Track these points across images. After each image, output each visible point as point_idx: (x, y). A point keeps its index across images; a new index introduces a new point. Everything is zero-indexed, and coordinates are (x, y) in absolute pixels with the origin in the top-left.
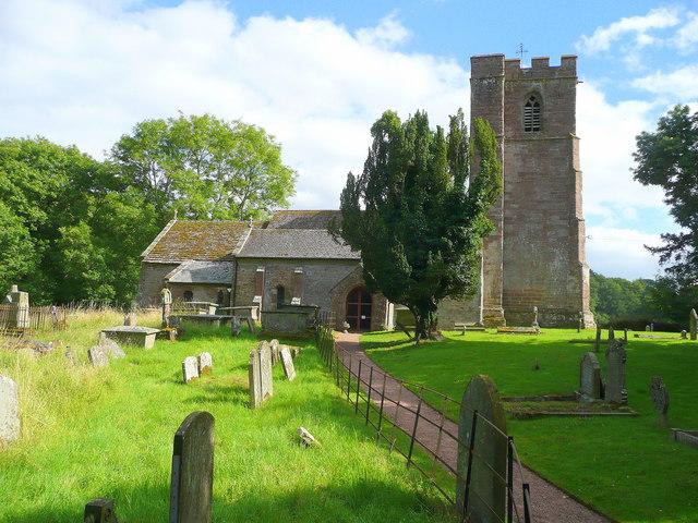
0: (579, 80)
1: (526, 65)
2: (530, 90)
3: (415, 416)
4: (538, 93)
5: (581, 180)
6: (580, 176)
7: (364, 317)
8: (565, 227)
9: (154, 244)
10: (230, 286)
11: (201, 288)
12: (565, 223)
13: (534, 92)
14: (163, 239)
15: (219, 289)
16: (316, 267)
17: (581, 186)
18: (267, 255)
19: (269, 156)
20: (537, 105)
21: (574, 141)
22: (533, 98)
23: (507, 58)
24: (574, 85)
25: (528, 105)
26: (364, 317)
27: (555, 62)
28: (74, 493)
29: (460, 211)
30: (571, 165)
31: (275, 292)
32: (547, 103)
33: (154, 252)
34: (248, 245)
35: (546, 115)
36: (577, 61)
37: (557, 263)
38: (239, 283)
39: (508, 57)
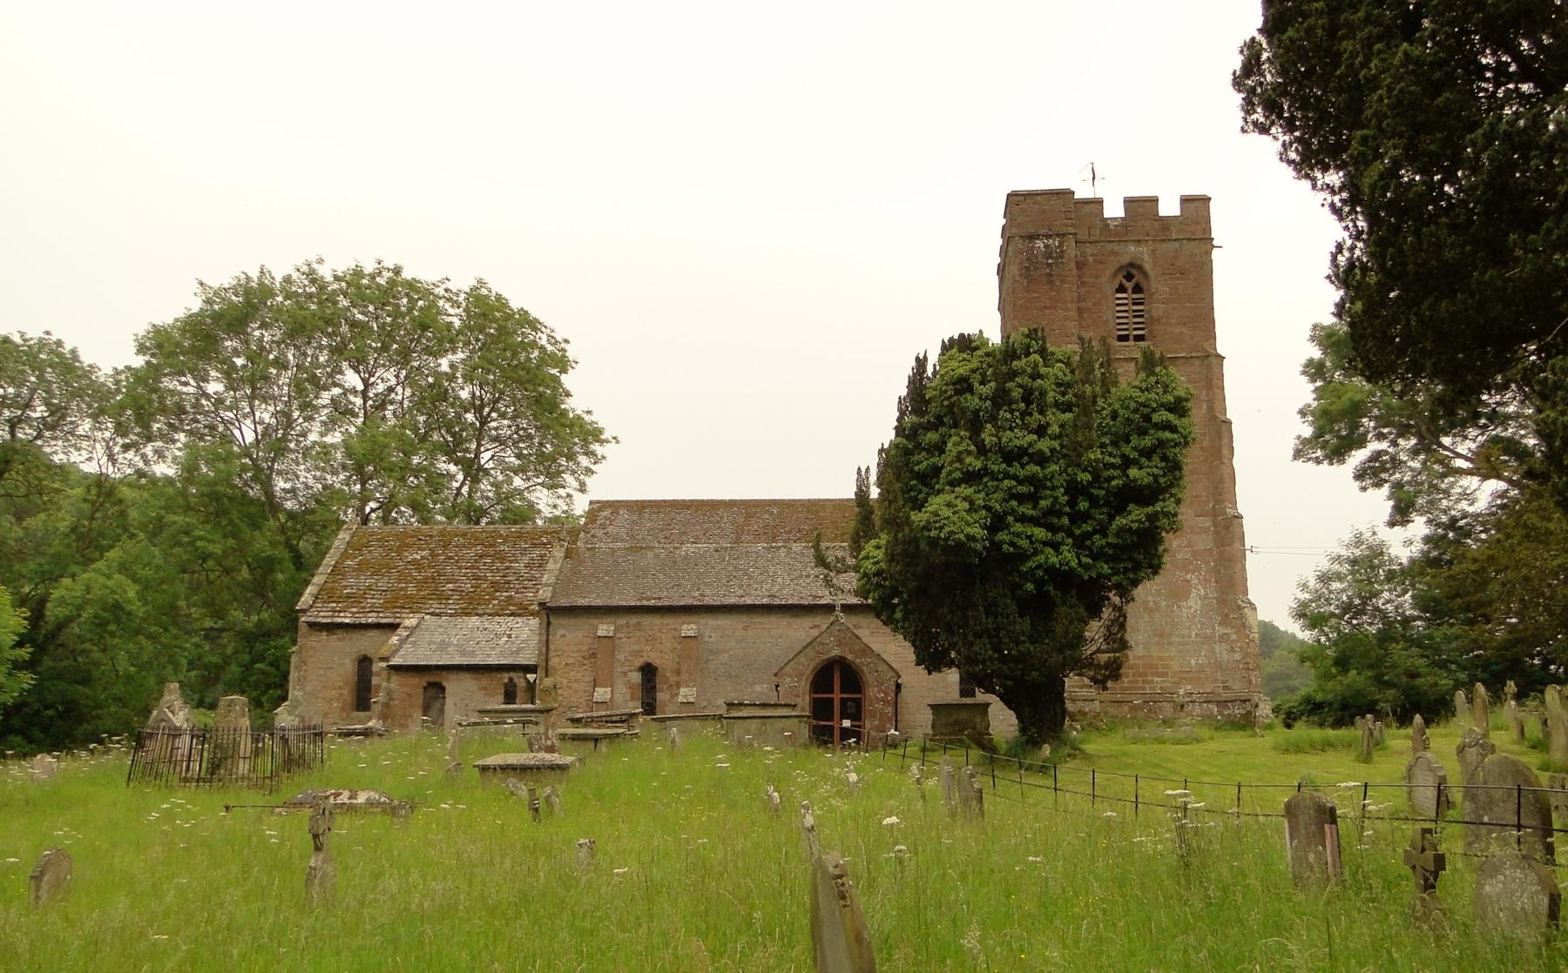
0: (1215, 243)
1: (1114, 210)
2: (1125, 260)
3: (1522, 823)
4: (1140, 268)
7: (847, 723)
9: (318, 579)
14: (337, 569)
15: (506, 677)
16: (724, 622)
19: (1179, 400)
20: (1138, 289)
22: (1129, 277)
25: (1121, 289)
27: (1169, 208)
31: (636, 677)
32: (1158, 286)
33: (327, 594)
35: (1158, 309)
37: (1194, 603)
38: (554, 662)
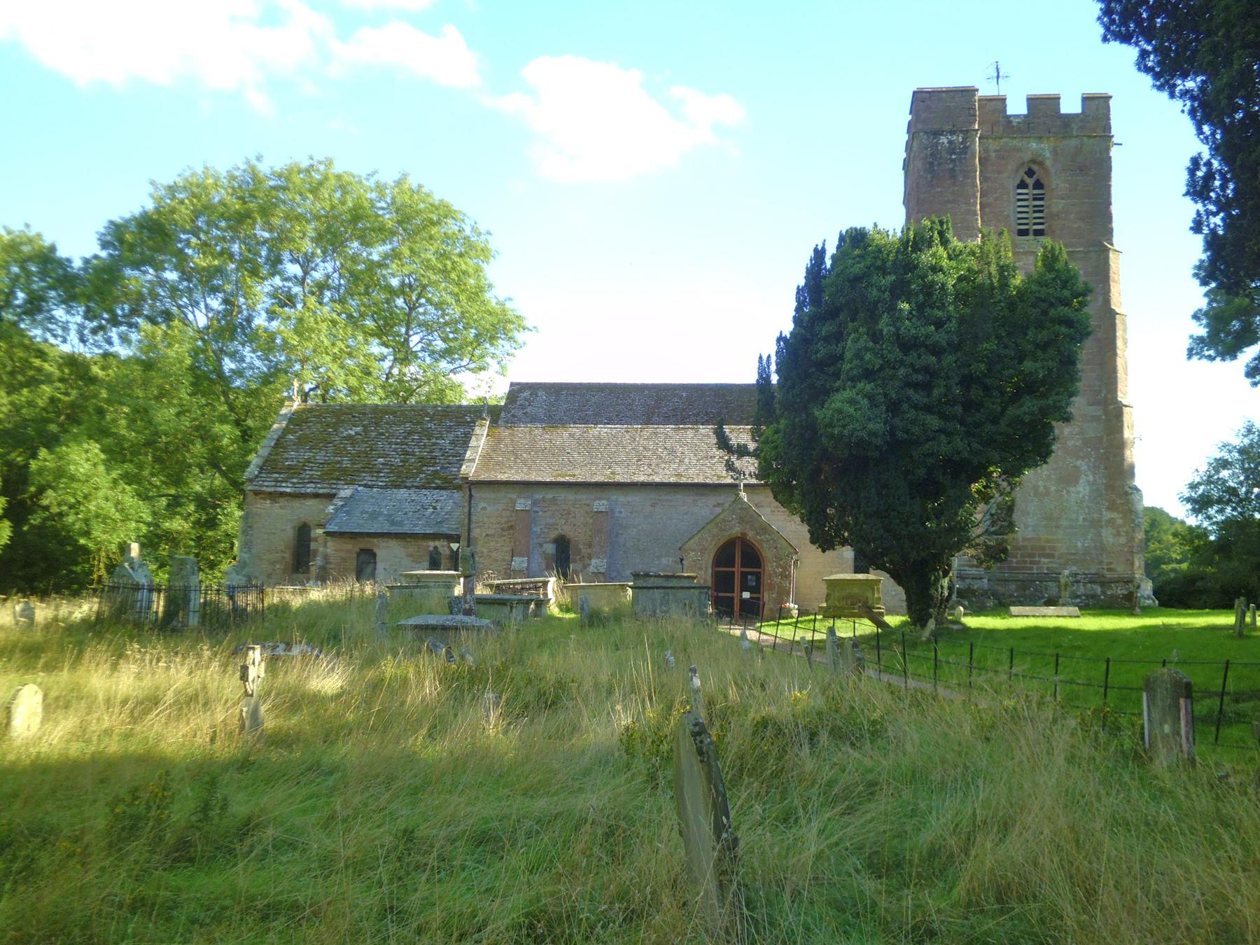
0: (1115, 140)
1: (1017, 107)
2: (1028, 156)
4: (1041, 164)
5: (1125, 331)
6: (1124, 324)
7: (746, 595)
8: (1096, 419)
10: (456, 539)
11: (393, 543)
12: (1099, 412)
13: (1033, 161)
15: (432, 544)
16: (634, 498)
17: (1125, 343)
18: (533, 477)
20: (1038, 185)
21: (1111, 255)
23: (981, 93)
24: (1108, 149)
25: (1023, 185)
26: (746, 595)
27: (1071, 106)
28: (407, 186)
29: (1089, 334)
30: (1107, 301)
31: (550, 548)
32: (1058, 183)
34: (486, 458)
36: (1112, 102)
38: (476, 532)
39: (983, 92)
